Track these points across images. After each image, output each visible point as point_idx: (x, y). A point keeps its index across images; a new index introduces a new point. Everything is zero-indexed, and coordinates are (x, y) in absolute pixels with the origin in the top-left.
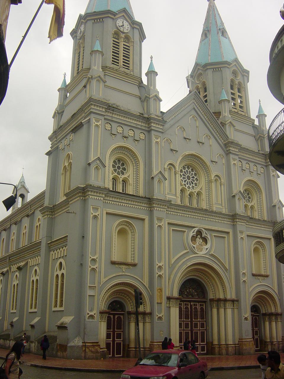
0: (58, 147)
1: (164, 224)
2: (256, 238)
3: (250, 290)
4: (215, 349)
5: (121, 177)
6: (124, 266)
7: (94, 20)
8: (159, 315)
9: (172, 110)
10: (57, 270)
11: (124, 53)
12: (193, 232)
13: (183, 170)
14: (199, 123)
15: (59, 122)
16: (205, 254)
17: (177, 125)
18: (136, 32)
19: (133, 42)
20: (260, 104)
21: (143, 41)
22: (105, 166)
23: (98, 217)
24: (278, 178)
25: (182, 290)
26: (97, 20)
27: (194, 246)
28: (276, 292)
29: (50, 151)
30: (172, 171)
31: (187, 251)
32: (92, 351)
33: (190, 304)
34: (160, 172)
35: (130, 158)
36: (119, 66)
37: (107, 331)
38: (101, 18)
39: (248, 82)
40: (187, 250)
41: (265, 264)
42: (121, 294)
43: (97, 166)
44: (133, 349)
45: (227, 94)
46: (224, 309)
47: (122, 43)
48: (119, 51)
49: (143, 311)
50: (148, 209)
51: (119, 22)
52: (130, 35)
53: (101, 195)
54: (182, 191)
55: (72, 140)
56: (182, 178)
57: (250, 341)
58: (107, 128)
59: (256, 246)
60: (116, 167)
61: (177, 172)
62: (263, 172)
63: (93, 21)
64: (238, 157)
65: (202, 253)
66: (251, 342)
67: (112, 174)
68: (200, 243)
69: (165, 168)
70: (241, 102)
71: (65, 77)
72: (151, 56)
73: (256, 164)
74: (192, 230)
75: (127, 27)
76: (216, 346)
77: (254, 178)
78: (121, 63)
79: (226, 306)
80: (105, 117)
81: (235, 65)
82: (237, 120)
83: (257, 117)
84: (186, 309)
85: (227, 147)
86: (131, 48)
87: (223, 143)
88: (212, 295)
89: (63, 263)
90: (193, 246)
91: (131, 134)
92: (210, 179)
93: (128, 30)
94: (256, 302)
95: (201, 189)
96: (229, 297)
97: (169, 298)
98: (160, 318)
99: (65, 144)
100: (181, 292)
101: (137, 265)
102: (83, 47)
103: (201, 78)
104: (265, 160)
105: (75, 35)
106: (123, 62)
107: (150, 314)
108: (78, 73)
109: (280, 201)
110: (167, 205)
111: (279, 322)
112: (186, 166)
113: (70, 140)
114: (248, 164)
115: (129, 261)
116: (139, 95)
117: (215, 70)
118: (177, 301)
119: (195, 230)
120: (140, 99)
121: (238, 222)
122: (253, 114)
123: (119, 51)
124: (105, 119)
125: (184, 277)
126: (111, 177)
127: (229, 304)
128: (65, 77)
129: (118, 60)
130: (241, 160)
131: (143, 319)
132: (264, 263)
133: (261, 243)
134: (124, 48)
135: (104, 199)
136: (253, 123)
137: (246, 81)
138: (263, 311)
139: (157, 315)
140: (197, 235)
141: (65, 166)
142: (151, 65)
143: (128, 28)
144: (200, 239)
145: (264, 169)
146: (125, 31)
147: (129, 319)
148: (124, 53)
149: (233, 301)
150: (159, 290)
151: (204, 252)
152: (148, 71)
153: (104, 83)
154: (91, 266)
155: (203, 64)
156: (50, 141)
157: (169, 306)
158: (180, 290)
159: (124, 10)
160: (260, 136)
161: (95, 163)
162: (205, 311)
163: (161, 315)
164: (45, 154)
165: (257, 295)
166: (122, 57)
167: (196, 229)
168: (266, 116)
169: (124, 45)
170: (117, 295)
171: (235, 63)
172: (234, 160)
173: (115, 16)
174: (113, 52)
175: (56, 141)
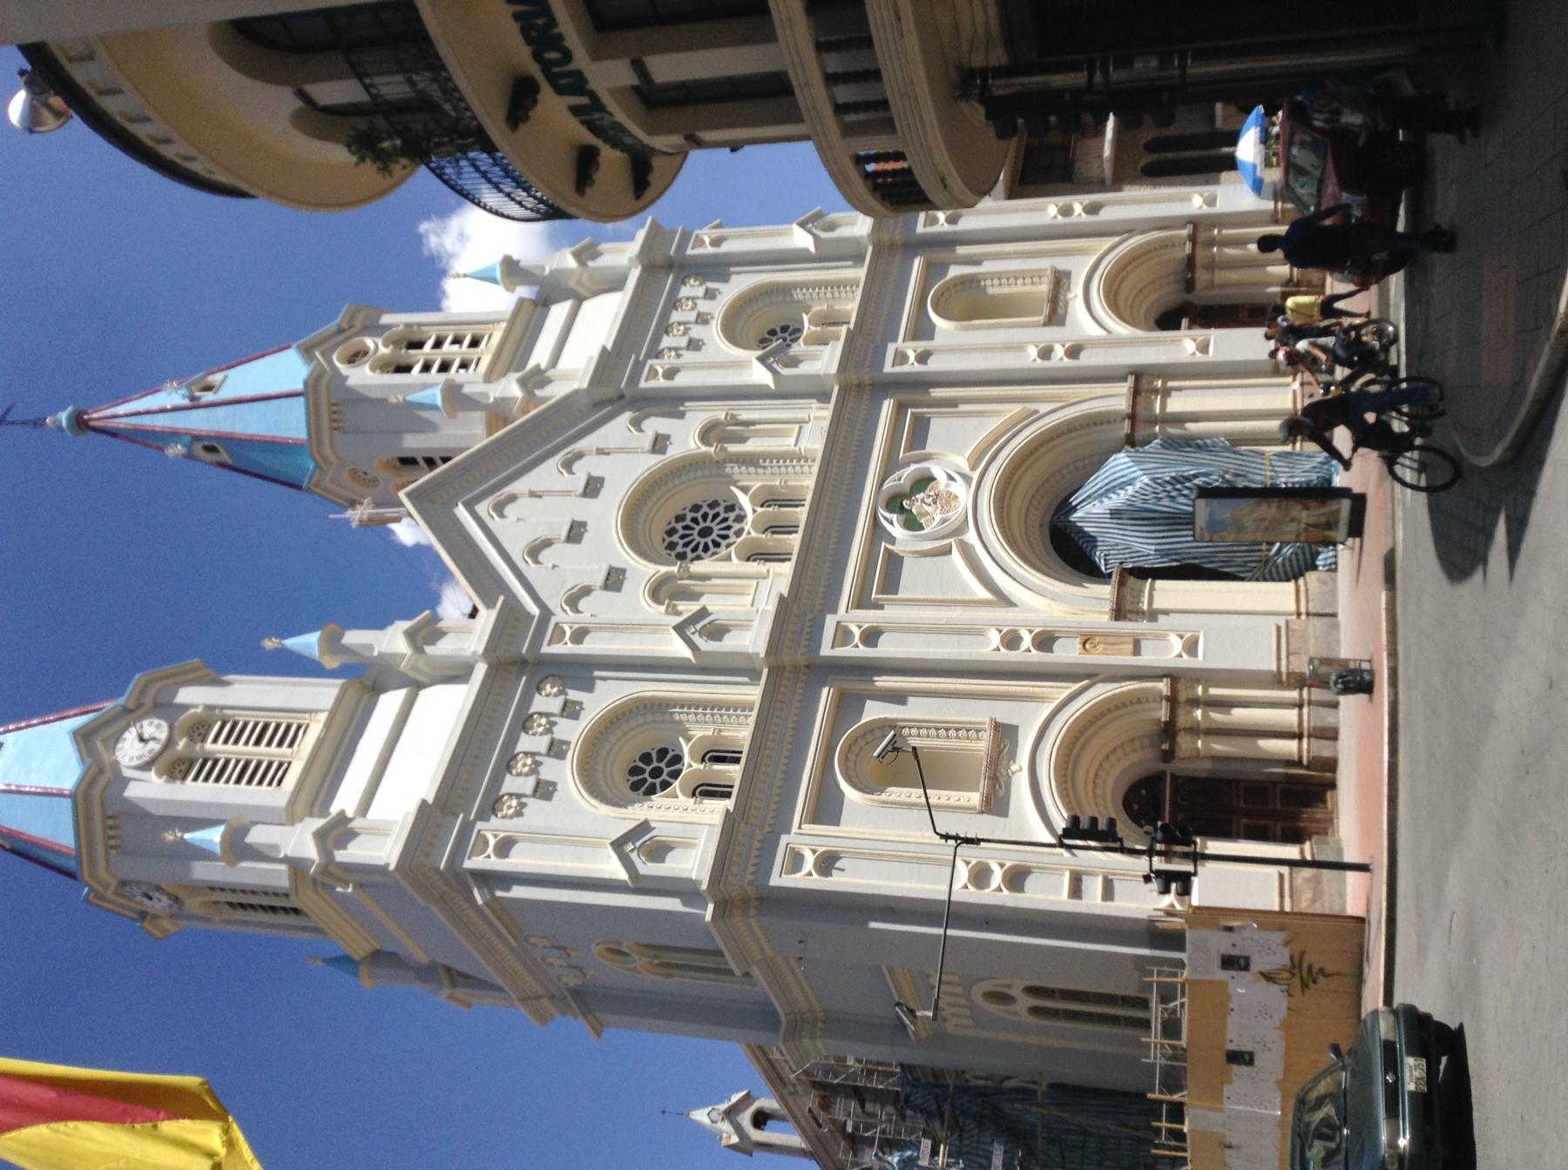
1: (858, 620)
5: (691, 765)
9: (150, 391)
10: (1016, 1013)
11: (247, 743)
12: (892, 523)
13: (679, 549)
42: (1099, 792)
44: (1305, 745)
45: (425, 386)
47: (209, 746)
48: (238, 762)
56: (703, 554)
60: (653, 781)
70: (457, 341)
73: (674, 303)
89: (987, 986)
97: (1119, 613)
103: (366, 473)
106: (280, 744)
112: (664, 540)
123: (238, 762)
129: (259, 764)
132: (1000, 285)
134: (226, 741)
140: (902, 510)
142: (968, 494)
148: (247, 743)
149: (1136, 392)
150: (1087, 646)
151: (958, 488)
166: (273, 749)
167: (882, 512)
169: (215, 740)
174: (238, 781)
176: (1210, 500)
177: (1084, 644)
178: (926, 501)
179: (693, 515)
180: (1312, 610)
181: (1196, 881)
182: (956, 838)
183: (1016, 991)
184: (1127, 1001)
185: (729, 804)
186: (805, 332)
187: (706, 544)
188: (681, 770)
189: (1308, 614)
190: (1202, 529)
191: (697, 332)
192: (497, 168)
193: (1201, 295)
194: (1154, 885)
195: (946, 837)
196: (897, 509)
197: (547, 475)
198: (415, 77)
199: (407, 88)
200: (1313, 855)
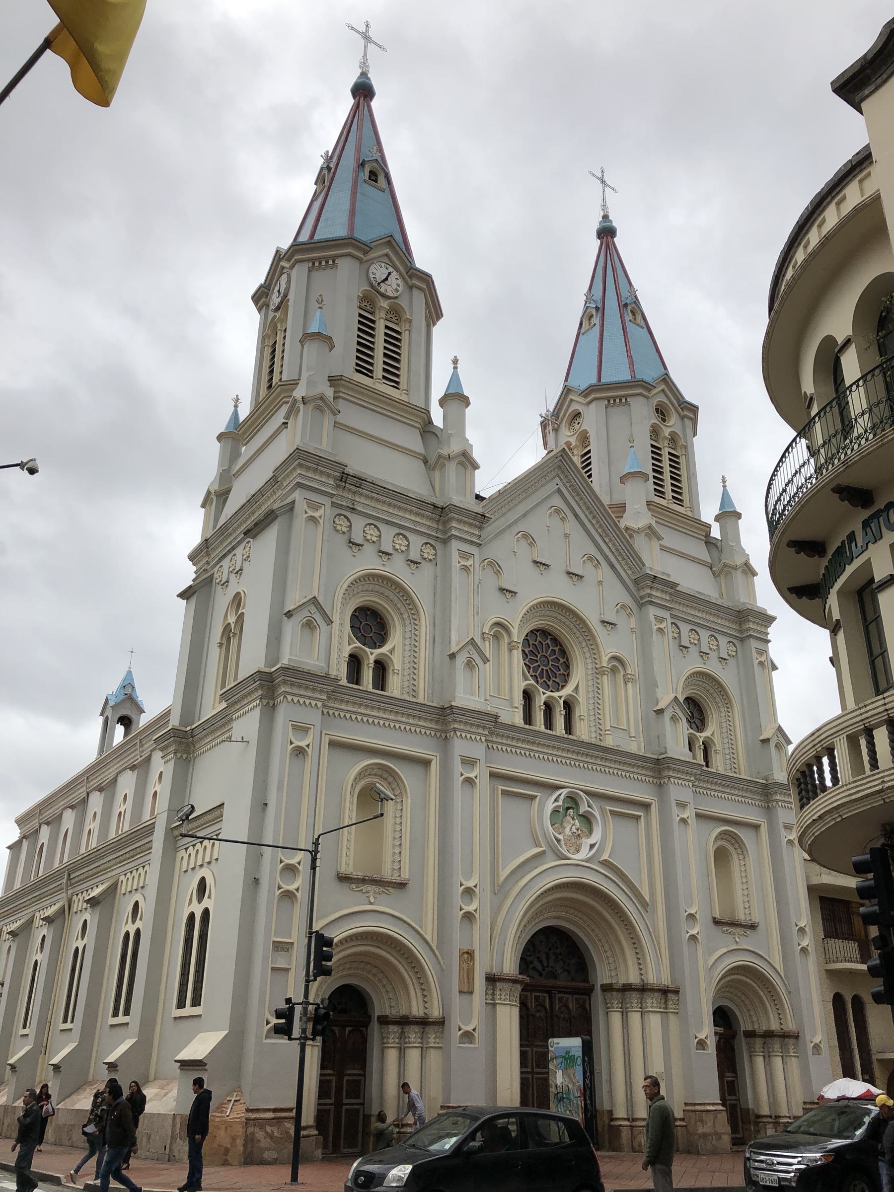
0: (211, 578)
1: (479, 773)
2: (721, 823)
3: (711, 962)
4: (620, 1131)
5: (371, 655)
6: (369, 888)
7: (313, 261)
8: (466, 1028)
12: (556, 800)
14: (571, 524)
15: (216, 520)
16: (587, 861)
17: (515, 529)
18: (419, 299)
19: (410, 321)
20: (724, 487)
21: (434, 324)
22: (329, 622)
23: (306, 752)
24: (773, 670)
25: (529, 959)
26: (320, 263)
27: (560, 837)
28: (779, 970)
29: (190, 587)
30: (501, 643)
31: (541, 849)
32: (271, 1136)
34: (472, 642)
35: (396, 605)
37: (319, 1104)
38: (330, 257)
39: (695, 434)
40: (541, 847)
41: (746, 892)
43: (309, 620)
46: (780, 1058)
49: (421, 1014)
50: (438, 734)
51: (379, 271)
52: (404, 303)
53: (317, 695)
54: (527, 696)
55: (248, 557)
57: (716, 1110)
58: (339, 527)
59: (719, 843)
61: (514, 644)
62: (734, 654)
64: (668, 613)
65: (580, 858)
66: (718, 1115)
67: (349, 644)
68: (574, 830)
69: (483, 634)
71: (236, 407)
72: (456, 357)
73: (715, 633)
74: (551, 794)
75: (394, 285)
76: (622, 1123)
77: (713, 667)
78: (378, 371)
79: (647, 1007)
80: (334, 500)
81: (663, 390)
82: (669, 525)
83: (717, 519)
85: (643, 588)
86: (405, 337)
87: (630, 579)
88: (608, 974)
89: (209, 882)
90: (554, 836)
91: (400, 545)
92: (597, 666)
93: (397, 290)
94: (723, 997)
95: (577, 688)
96: (652, 979)
97: (492, 980)
98: (468, 1036)
99: (231, 570)
100: (525, 963)
101: (406, 884)
102: (283, 329)
104: (738, 625)
105: (264, 299)
106: (384, 370)
107: (441, 1023)
108: (270, 387)
109: (780, 729)
110: (488, 726)
111: (793, 1059)
113: (244, 557)
114: (696, 632)
115: (387, 873)
116: (422, 451)
117: (612, 401)
118: (513, 989)
119: (560, 795)
120: (426, 462)
121: (673, 777)
122: (708, 512)
124: (334, 504)
125: (533, 923)
126: (347, 650)
127: (655, 1002)
128: (236, 407)
130: (675, 621)
131: (422, 1038)
133: (735, 837)
134: (385, 370)
135: (324, 706)
136: (708, 535)
137: (689, 431)
138: (745, 1025)
139: (459, 1027)
141: (229, 624)
142: (455, 379)
143: (398, 285)
144: (573, 818)
145: (735, 646)
146: (390, 294)
147: (383, 1038)
149: (665, 992)
150: (466, 956)
151: (584, 853)
152: (445, 394)
153: (335, 414)
154: (282, 885)
155: (583, 388)
156: (193, 564)
157: (492, 1002)
158: (521, 958)
159: (390, 241)
160: (725, 566)
161: (305, 613)
163: (469, 1028)
164: (178, 596)
165: (728, 978)
167: (564, 792)
168: (738, 516)
170: (357, 968)
171: (663, 387)
172: (660, 620)
175: (208, 563)
176: (581, 1049)
177: (467, 953)
178: (574, 827)
181: (283, 1041)
183: (206, 903)
186: (697, 734)
190: (558, 1043)
192: (803, 481)
193: (742, 1044)
194: (283, 1006)
195: (316, 843)
196: (566, 805)
197: (581, 545)
198: (866, 416)
199: (858, 410)
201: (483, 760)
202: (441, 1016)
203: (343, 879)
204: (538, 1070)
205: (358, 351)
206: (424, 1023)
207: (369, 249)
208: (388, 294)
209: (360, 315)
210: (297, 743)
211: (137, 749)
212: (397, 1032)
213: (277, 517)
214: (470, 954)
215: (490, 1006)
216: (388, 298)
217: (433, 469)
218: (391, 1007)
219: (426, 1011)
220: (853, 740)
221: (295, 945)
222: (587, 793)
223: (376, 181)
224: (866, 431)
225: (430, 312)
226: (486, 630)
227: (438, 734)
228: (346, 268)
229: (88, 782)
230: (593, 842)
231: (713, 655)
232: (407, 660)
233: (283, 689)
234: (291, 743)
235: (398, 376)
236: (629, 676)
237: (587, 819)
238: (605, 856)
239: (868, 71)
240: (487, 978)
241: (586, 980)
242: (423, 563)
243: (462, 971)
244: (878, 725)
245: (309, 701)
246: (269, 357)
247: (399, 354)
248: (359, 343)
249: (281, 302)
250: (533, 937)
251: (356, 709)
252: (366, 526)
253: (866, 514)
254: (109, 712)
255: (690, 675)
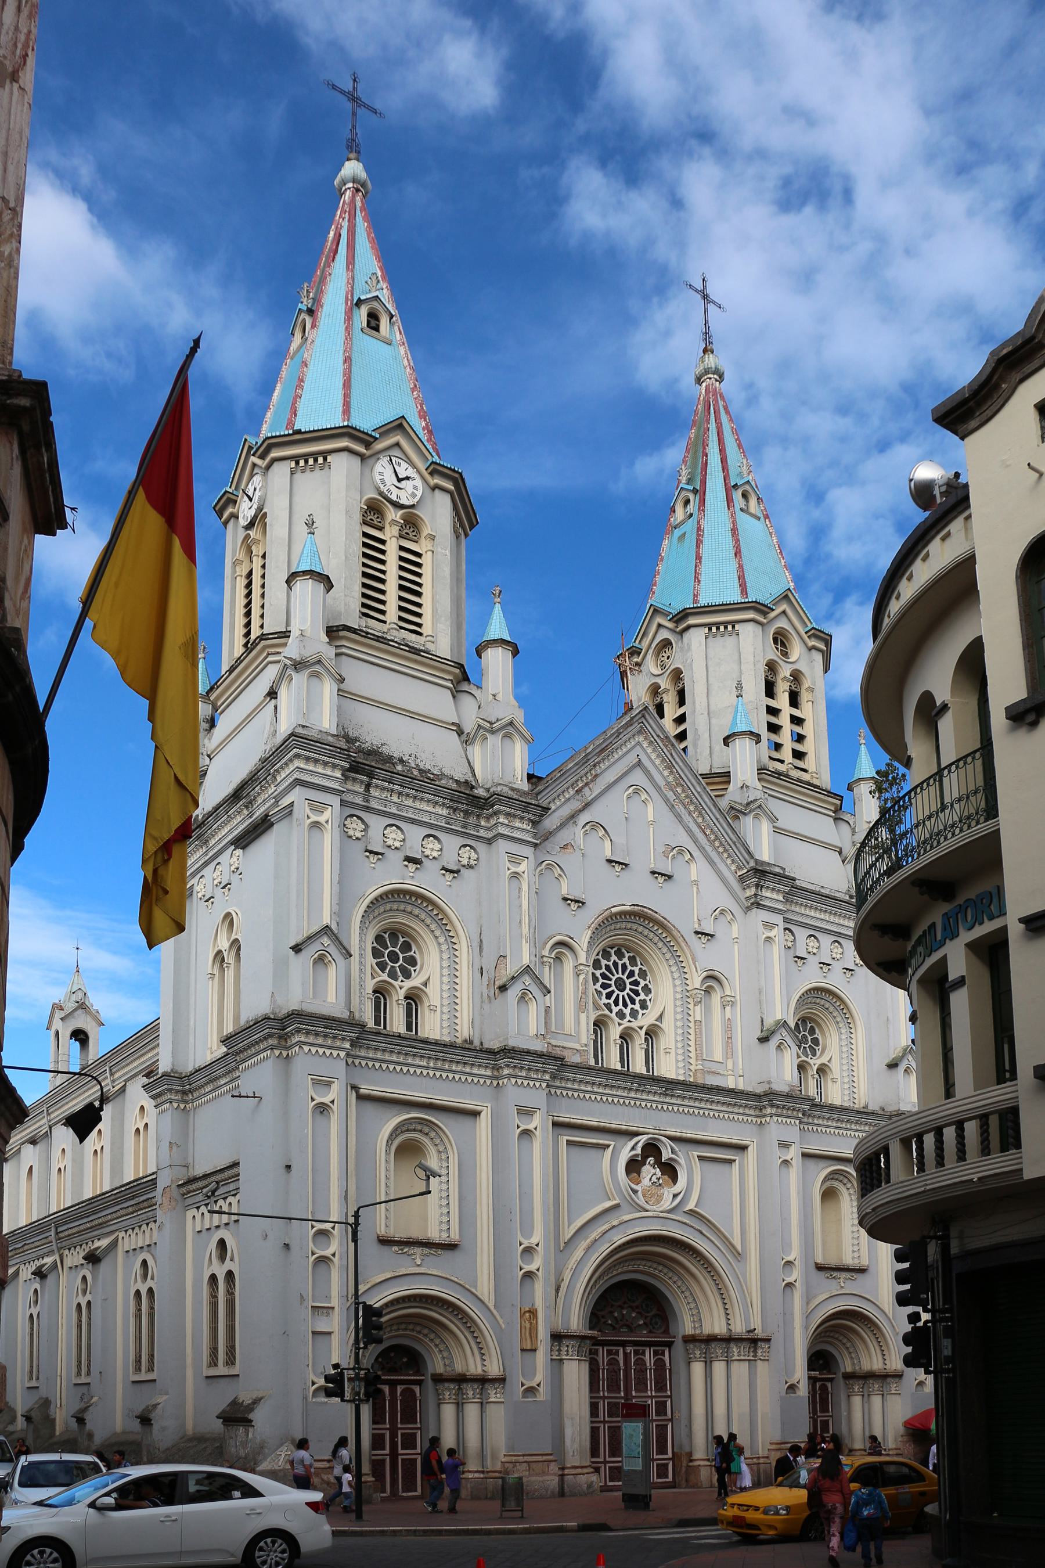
7: (296, 459)
12: (633, 1148)
13: (604, 962)
16: (670, 1211)
33: (624, 1351)
36: (385, 622)
49: (479, 1371)
50: (488, 1082)
58: (351, 833)
63: (293, 464)
65: (661, 1209)
81: (784, 612)
84: (611, 1364)
92: (689, 988)
93: (414, 495)
97: (557, 1337)
99: (216, 882)
102: (261, 554)
110: (549, 1071)
119: (637, 1143)
120: (460, 732)
126: (370, 985)
131: (481, 1394)
146: (404, 501)
147: (439, 1395)
150: (527, 1314)
151: (667, 1203)
154: (317, 1251)
162: (670, 1370)
167: (643, 1139)
173: (368, 445)
179: (637, 972)
180: (566, 1478)
182: (357, 1223)
184: (231, 1349)
185: (371, 1024)
187: (610, 986)
188: (396, 980)
189: (562, 1475)
191: (813, 962)
195: (356, 1215)
200: (366, 1482)
201: (544, 1109)
202: (502, 1373)
203: (385, 1242)
204: (611, 1419)
205: (364, 585)
206: (483, 1381)
207: (371, 440)
208: (401, 502)
209: (365, 535)
210: (319, 1100)
211: (107, 1077)
212: (454, 1389)
213: (272, 824)
214: (533, 1313)
215: (555, 1363)
216: (402, 507)
217: (472, 743)
218: (445, 1365)
219: (484, 1368)
220: (906, 1143)
221: (336, 1309)
222: (672, 1138)
223: (377, 329)
224: (945, 829)
225: (460, 519)
226: (546, 953)
227: (488, 1082)
228: (342, 466)
229: (49, 1114)
230: (676, 1192)
231: (837, 967)
232: (445, 995)
233: (297, 1039)
234: (313, 1100)
235: (419, 615)
236: (729, 999)
237: (670, 1170)
238: (691, 1205)
239: (971, 403)
240: (551, 1335)
241: (666, 1332)
242: (463, 870)
243: (523, 1330)
244: (928, 1131)
245: (330, 1051)
246: (245, 592)
247: (420, 585)
248: (365, 575)
249: (255, 517)
250: (605, 1291)
251: (387, 1057)
252: (385, 828)
253: (945, 907)
254: (57, 1024)
255: (806, 992)
